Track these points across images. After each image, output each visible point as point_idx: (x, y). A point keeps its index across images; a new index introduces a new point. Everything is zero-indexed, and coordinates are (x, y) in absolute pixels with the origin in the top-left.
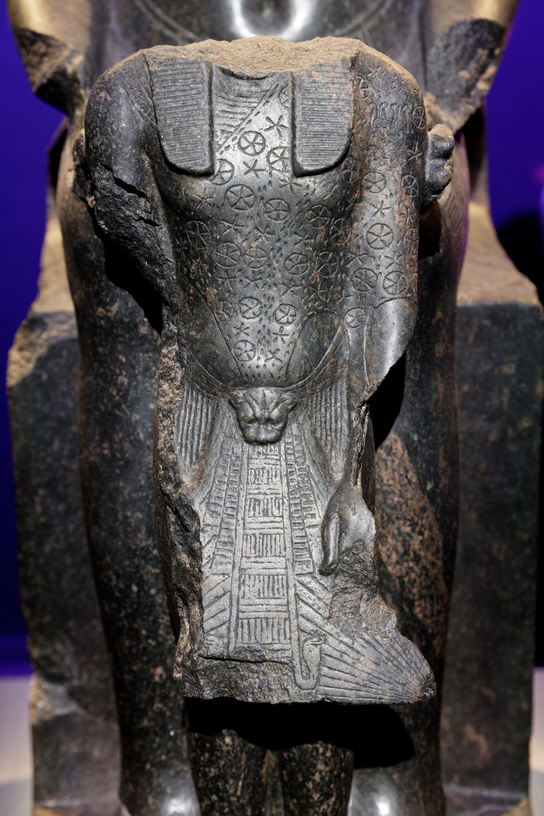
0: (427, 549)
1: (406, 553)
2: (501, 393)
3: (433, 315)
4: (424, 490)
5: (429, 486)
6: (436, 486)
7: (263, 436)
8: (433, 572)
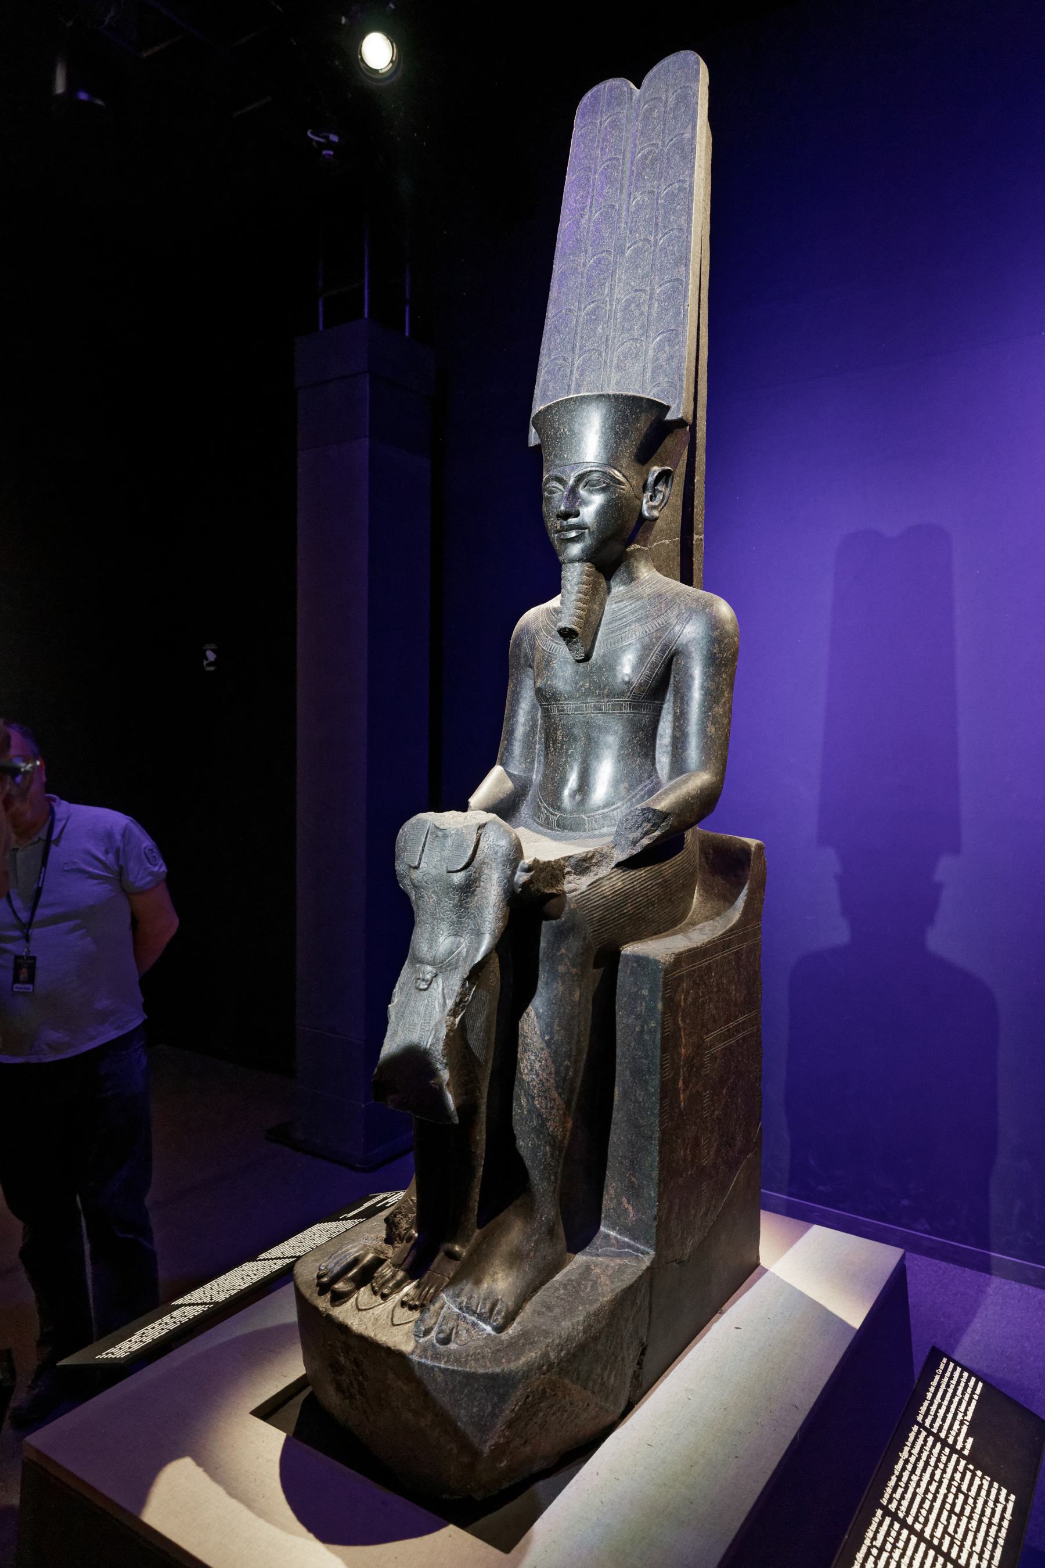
0: (543, 1070)
1: (531, 1070)
2: (641, 1005)
3: (558, 949)
4: (543, 1039)
5: (547, 1038)
6: (551, 1039)
7: (422, 987)
8: (547, 1084)
